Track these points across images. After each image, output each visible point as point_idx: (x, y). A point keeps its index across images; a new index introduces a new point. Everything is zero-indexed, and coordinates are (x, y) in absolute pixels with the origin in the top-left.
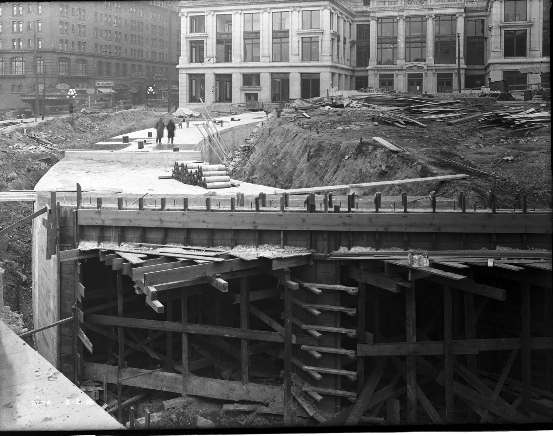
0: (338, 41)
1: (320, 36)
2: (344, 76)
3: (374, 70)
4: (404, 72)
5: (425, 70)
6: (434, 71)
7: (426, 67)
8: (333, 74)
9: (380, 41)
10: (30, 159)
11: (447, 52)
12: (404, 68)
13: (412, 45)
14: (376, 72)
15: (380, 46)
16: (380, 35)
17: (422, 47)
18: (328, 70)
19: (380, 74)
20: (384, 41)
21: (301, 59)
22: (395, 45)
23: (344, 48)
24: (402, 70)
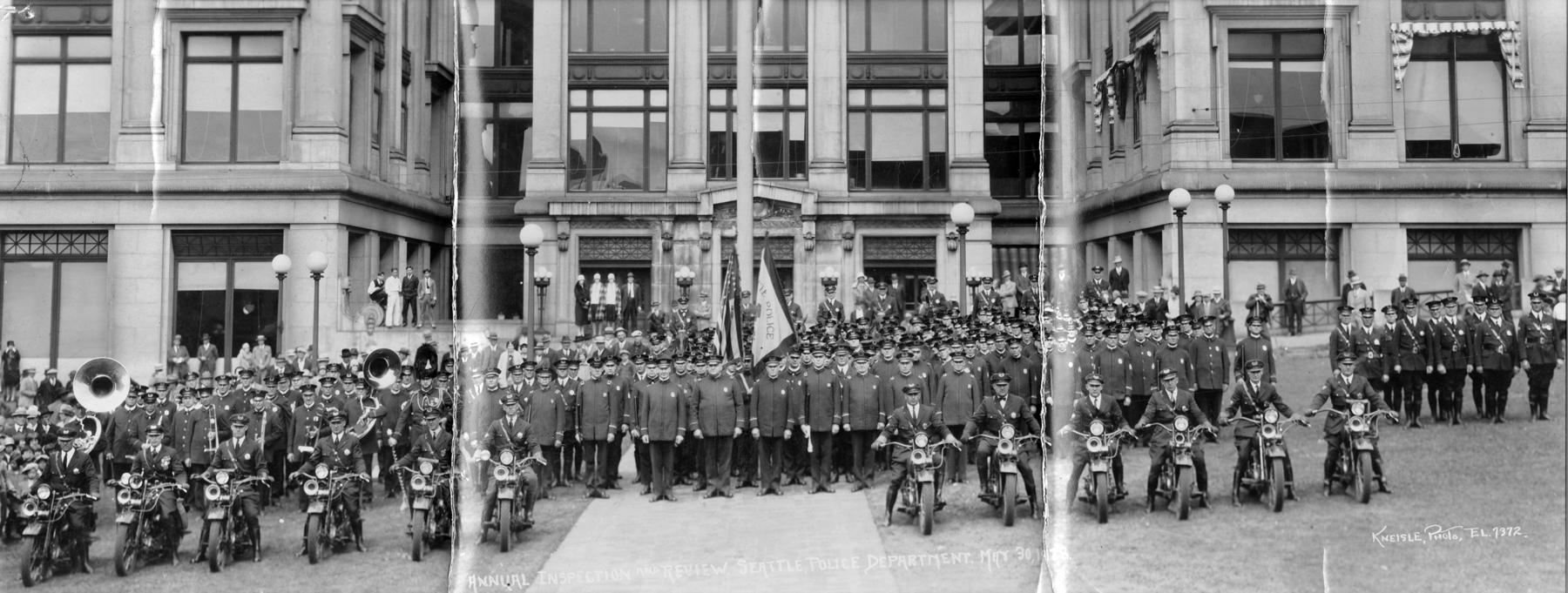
0: (379, 66)
1: (288, 29)
2: (403, 246)
3: (555, 219)
4: (705, 227)
5: (805, 218)
6: (848, 226)
7: (809, 208)
8: (356, 235)
9: (580, 71)
10: (1385, 568)
11: (1310, 141)
12: (706, 208)
13: (881, 98)
14: (563, 227)
15: (858, 97)
16: (581, 49)
17: (926, 110)
18: (332, 210)
19: (866, 238)
20: (601, 72)
21: (175, 149)
22: (936, 97)
23: (404, 106)
24: (693, 219)
